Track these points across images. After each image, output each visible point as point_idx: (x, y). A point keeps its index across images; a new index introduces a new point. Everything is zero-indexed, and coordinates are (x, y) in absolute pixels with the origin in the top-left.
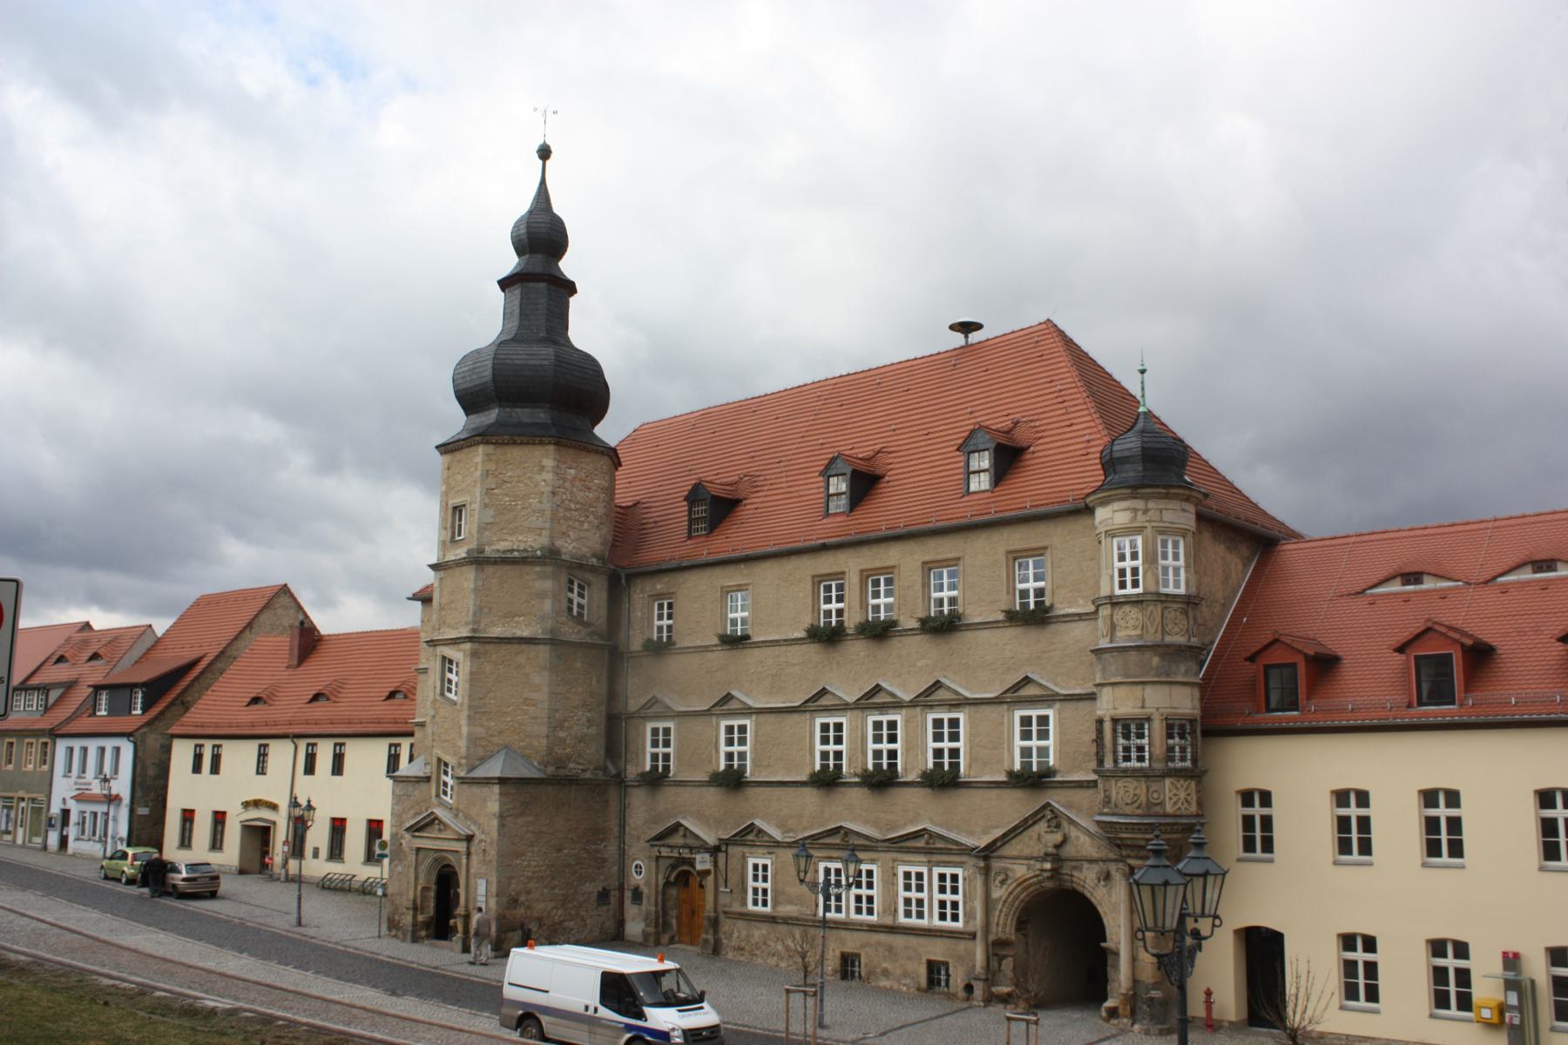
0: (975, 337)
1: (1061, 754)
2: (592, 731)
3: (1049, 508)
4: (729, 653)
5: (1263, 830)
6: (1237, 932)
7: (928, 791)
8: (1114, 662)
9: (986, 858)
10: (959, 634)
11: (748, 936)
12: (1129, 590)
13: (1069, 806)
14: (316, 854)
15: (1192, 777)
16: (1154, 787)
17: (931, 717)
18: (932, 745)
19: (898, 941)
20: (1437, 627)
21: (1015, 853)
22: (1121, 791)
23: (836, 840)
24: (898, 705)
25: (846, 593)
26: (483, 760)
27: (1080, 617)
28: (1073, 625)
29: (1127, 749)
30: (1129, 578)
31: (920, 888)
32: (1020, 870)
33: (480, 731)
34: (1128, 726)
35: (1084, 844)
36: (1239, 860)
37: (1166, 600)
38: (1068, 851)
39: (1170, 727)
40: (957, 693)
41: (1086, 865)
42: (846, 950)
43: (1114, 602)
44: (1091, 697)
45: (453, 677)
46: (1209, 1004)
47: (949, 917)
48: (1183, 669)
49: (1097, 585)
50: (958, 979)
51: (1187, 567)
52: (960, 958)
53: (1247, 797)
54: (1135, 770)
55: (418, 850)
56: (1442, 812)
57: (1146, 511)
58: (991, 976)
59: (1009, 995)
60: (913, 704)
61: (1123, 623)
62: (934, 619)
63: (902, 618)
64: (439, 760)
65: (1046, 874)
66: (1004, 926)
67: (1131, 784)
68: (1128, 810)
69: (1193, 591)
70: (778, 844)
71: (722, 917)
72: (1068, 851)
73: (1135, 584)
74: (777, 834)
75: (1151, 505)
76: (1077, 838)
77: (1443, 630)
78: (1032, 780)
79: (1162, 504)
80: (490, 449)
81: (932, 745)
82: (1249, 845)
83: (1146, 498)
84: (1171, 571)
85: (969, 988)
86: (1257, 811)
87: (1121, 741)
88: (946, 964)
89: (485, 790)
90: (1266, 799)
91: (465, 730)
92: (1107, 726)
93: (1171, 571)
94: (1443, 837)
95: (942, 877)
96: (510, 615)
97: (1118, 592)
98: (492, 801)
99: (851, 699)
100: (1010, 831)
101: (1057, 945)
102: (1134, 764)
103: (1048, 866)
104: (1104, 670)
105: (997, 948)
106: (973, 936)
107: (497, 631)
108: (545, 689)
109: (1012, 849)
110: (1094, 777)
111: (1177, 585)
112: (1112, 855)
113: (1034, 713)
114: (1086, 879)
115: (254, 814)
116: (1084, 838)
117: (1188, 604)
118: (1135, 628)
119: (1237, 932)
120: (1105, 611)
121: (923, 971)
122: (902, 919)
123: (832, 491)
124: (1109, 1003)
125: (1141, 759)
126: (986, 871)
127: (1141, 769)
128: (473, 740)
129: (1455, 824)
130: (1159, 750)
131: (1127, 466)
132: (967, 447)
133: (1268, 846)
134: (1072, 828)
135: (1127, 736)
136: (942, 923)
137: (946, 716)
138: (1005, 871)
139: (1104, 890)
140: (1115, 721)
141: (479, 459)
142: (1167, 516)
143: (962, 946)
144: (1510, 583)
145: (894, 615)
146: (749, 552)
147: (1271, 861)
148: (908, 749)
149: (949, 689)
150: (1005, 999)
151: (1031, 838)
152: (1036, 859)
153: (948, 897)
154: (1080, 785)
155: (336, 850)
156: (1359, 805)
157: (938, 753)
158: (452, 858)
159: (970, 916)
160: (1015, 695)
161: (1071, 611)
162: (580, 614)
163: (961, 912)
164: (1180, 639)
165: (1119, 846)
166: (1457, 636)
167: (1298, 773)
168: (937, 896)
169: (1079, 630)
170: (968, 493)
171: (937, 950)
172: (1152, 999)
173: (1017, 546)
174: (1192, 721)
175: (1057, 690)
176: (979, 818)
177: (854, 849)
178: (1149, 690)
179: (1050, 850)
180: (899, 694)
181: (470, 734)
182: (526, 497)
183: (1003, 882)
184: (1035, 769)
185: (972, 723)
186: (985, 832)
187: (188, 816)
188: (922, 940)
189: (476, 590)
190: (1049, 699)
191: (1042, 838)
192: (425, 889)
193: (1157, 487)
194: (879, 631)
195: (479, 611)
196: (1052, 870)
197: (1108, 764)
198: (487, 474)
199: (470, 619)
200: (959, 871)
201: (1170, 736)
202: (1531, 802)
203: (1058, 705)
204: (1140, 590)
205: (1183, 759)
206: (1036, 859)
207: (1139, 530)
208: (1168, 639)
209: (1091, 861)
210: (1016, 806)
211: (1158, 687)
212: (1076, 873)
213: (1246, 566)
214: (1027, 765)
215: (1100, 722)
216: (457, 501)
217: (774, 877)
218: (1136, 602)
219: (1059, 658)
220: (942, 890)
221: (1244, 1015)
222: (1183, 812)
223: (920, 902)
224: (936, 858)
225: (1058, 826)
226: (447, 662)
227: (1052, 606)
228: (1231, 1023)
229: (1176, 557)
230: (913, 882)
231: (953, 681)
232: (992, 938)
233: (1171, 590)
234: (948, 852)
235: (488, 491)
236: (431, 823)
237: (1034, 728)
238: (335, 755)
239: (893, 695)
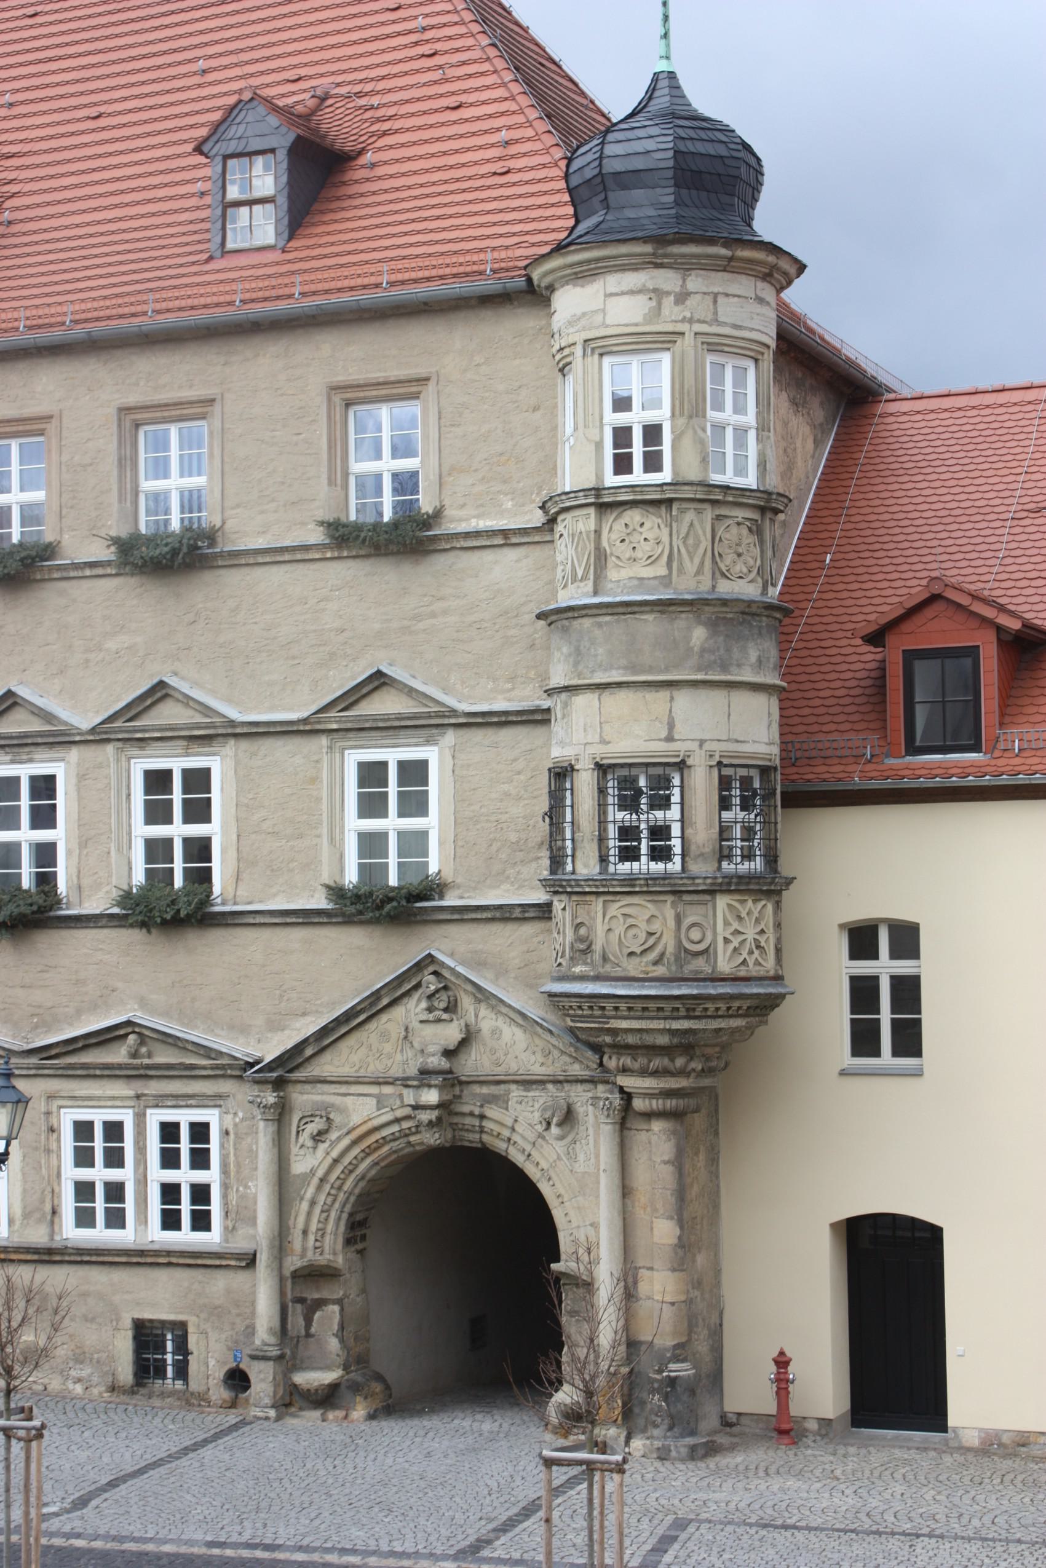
1: (458, 846)
3: (435, 289)
6: (834, 1226)
7: (136, 935)
8: (602, 642)
9: (279, 1084)
10: (208, 576)
12: (638, 476)
13: (479, 964)
15: (769, 893)
16: (581, 911)
17: (140, 765)
18: (142, 830)
19: (56, 1279)
20: (950, 594)
21: (346, 1071)
22: (618, 926)
24: (59, 739)
27: (506, 538)
28: (488, 556)
29: (627, 832)
30: (637, 450)
31: (115, 1159)
32: (361, 1110)
34: (636, 784)
35: (509, 1045)
36: (843, 1073)
37: (718, 498)
38: (474, 1063)
39: (725, 783)
40: (206, 710)
41: (516, 1092)
42: (147, 1315)
43: (604, 504)
44: (538, 718)
46: (782, 1384)
47: (186, 1219)
48: (753, 655)
49: (551, 467)
50: (209, 1361)
51: (762, 428)
52: (216, 1312)
53: (862, 939)
57: (682, 298)
58: (290, 1349)
59: (334, 1387)
60: (99, 736)
61: (624, 551)
62: (151, 540)
63: (67, 539)
65: (425, 1116)
66: (321, 1238)
67: (642, 910)
68: (633, 968)
69: (773, 482)
72: (474, 1063)
73: (653, 463)
75: (695, 282)
76: (496, 1032)
77: (964, 601)
78: (390, 905)
79: (719, 282)
81: (142, 830)
82: (864, 1040)
83: (685, 266)
84: (729, 433)
85: (237, 1379)
86: (885, 967)
87: (618, 816)
88: (180, 1330)
90: (906, 939)
92: (585, 782)
93: (729, 433)
95: (169, 1131)
97: (611, 480)
99: (84, 721)
100: (338, 1022)
101: (460, 1278)
102: (645, 865)
103: (431, 1096)
104: (578, 655)
105: (304, 1286)
106: (250, 1261)
109: (336, 1063)
110: (539, 896)
111: (740, 471)
112: (576, 1070)
113: (392, 755)
114: (518, 1128)
116: (512, 1036)
117: (763, 510)
118: (652, 560)
119: (834, 1226)
120: (584, 522)
121: (124, 1347)
122: (70, 1232)
123: (233, 192)
124: (566, 1396)
125: (660, 854)
126: (280, 1114)
127: (666, 876)
130: (704, 834)
131: (638, 194)
132: (217, 144)
133: (909, 1040)
134: (484, 1011)
135: (629, 803)
136: (171, 1236)
137: (177, 764)
138: (325, 1113)
139: (560, 1147)
140: (603, 769)
142: (729, 310)
143: (220, 1284)
145: (209, 517)
147: (918, 1073)
148: (83, 842)
149: (187, 701)
150: (326, 1399)
151: (385, 1036)
152: (405, 1082)
153: (185, 1176)
154: (503, 914)
156: (896, 954)
157: (158, 850)
159: (237, 1216)
160: (345, 715)
161: (483, 524)
163: (215, 1207)
164: (749, 590)
165: (598, 1049)
166: (989, 612)
168: (158, 1175)
169: (505, 567)
170: (225, 253)
171: (159, 1297)
172: (672, 1381)
173: (354, 374)
174: (765, 771)
175: (451, 702)
176: (256, 993)
178: (683, 700)
179: (436, 1061)
180: (64, 714)
183: (318, 1137)
184: (393, 881)
185: (243, 780)
186: (275, 1026)
188: (119, 1276)
190: (433, 722)
191: (412, 1036)
193: (711, 241)
194: (13, 566)
196: (440, 1106)
197: (586, 866)
200: (211, 1116)
201: (725, 804)
203: (450, 737)
204: (666, 475)
205: (748, 856)
206: (405, 1082)
207: (666, 340)
208: (725, 588)
209: (529, 1083)
210: (359, 961)
211: (703, 694)
212: (492, 1112)
213: (818, 443)
214: (370, 872)
215: (562, 774)
218: (659, 502)
219: (457, 631)
220: (170, 1160)
221: (845, 1405)
222: (753, 970)
223: (115, 1192)
225: (451, 1008)
227: (438, 514)
228: (824, 1423)
229: (739, 409)
230: (99, 1144)
231: (196, 684)
232: (294, 1263)
233: (728, 478)
234: (188, 1072)
237: (177, 796)
239: (47, 716)
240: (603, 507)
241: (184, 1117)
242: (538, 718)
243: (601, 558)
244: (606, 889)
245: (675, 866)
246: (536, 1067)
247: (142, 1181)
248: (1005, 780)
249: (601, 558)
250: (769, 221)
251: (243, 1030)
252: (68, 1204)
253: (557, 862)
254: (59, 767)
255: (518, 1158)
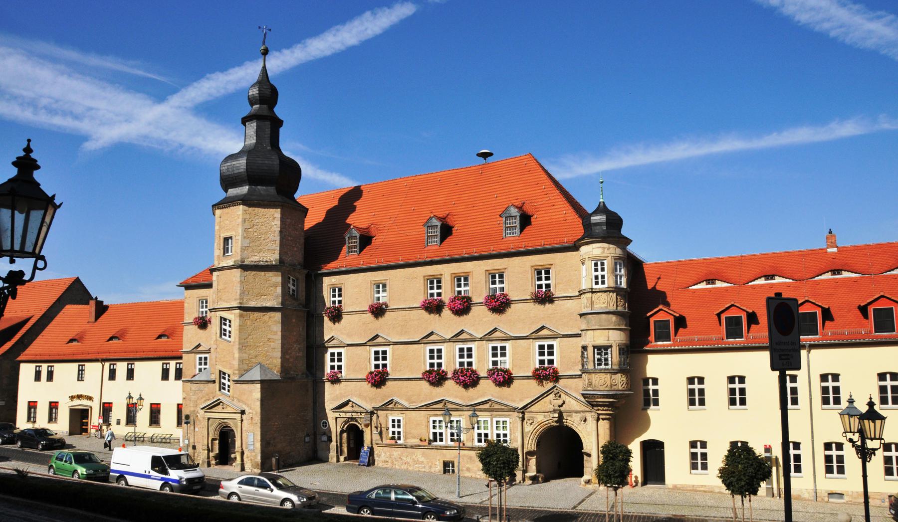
0: (490, 159)
2: (301, 354)
4: (452, 315)
5: (740, 395)
11: (390, 456)
14: (118, 422)
21: (537, 410)
23: (440, 406)
24: (473, 340)
25: (443, 284)
26: (247, 371)
29: (599, 360)
32: (540, 418)
33: (245, 356)
34: (601, 349)
35: (574, 405)
44: (578, 335)
45: (227, 328)
49: (580, 283)
54: (605, 369)
55: (209, 419)
56: (696, 386)
57: (609, 249)
64: (220, 371)
67: (603, 376)
68: (602, 388)
70: (407, 409)
71: (375, 447)
73: (603, 283)
74: (407, 404)
80: (246, 208)
87: (597, 357)
89: (251, 386)
91: (237, 355)
92: (590, 349)
94: (737, 397)
96: (260, 295)
98: (256, 391)
102: (603, 367)
107: (252, 304)
108: (280, 333)
110: (580, 373)
112: (587, 409)
114: (573, 422)
115: (77, 402)
116: (573, 402)
124: (586, 477)
125: (606, 364)
128: (241, 361)
129: (742, 391)
138: (532, 418)
140: (594, 347)
141: (240, 213)
144: (821, 280)
146: (411, 261)
155: (131, 419)
158: (231, 423)
160: (536, 335)
162: (293, 294)
167: (666, 369)
177: (449, 410)
181: (239, 358)
182: (267, 233)
183: (531, 424)
186: (521, 400)
187: (32, 406)
189: (241, 282)
191: (550, 403)
192: (213, 440)
195: (243, 292)
198: (245, 220)
199: (238, 297)
202: (685, 381)
204: (606, 286)
206: (551, 412)
215: (585, 348)
216: (227, 235)
217: (405, 425)
224: (495, 413)
226: (223, 320)
232: (525, 450)
235: (246, 230)
236: (219, 404)
238: (36, 372)
239: (471, 335)
240: (593, 292)
241: (501, 419)
242: (578, 335)
243: (592, 303)
244: (595, 372)
245: (609, 367)
246: (579, 409)
247: (492, 433)
248: (757, 345)
249: (592, 303)
250: (624, 232)
251: (514, 401)
252: (476, 438)
253: (583, 366)
254: (443, 347)
255: (574, 428)
